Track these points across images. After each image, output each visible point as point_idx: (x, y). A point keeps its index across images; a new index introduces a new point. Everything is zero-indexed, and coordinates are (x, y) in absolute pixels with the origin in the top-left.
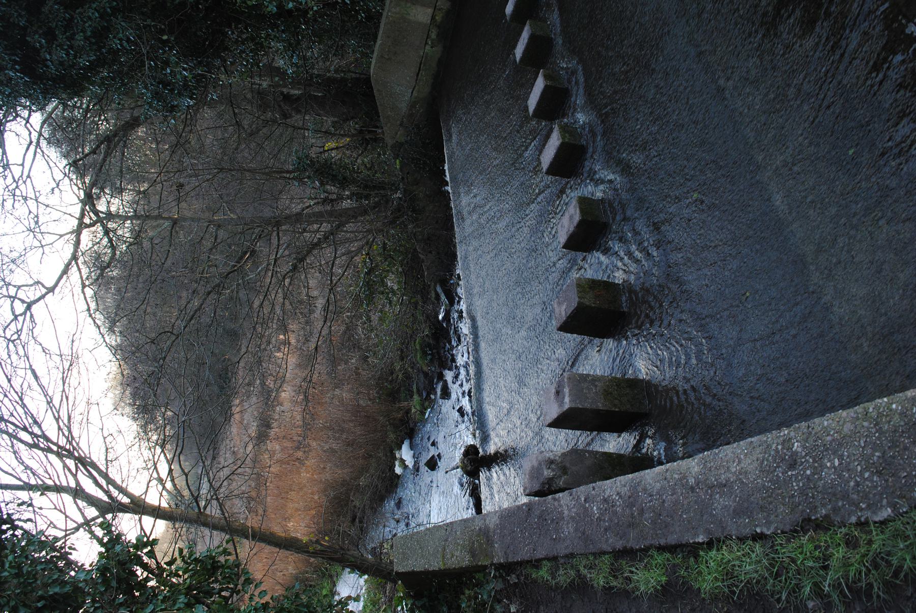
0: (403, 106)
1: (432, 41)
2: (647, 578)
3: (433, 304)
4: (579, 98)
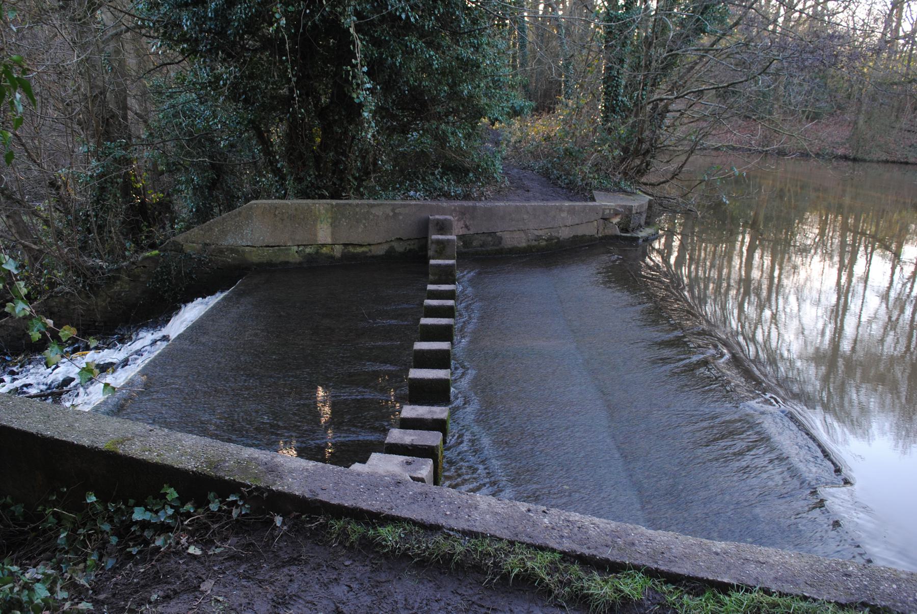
0: (230, 241)
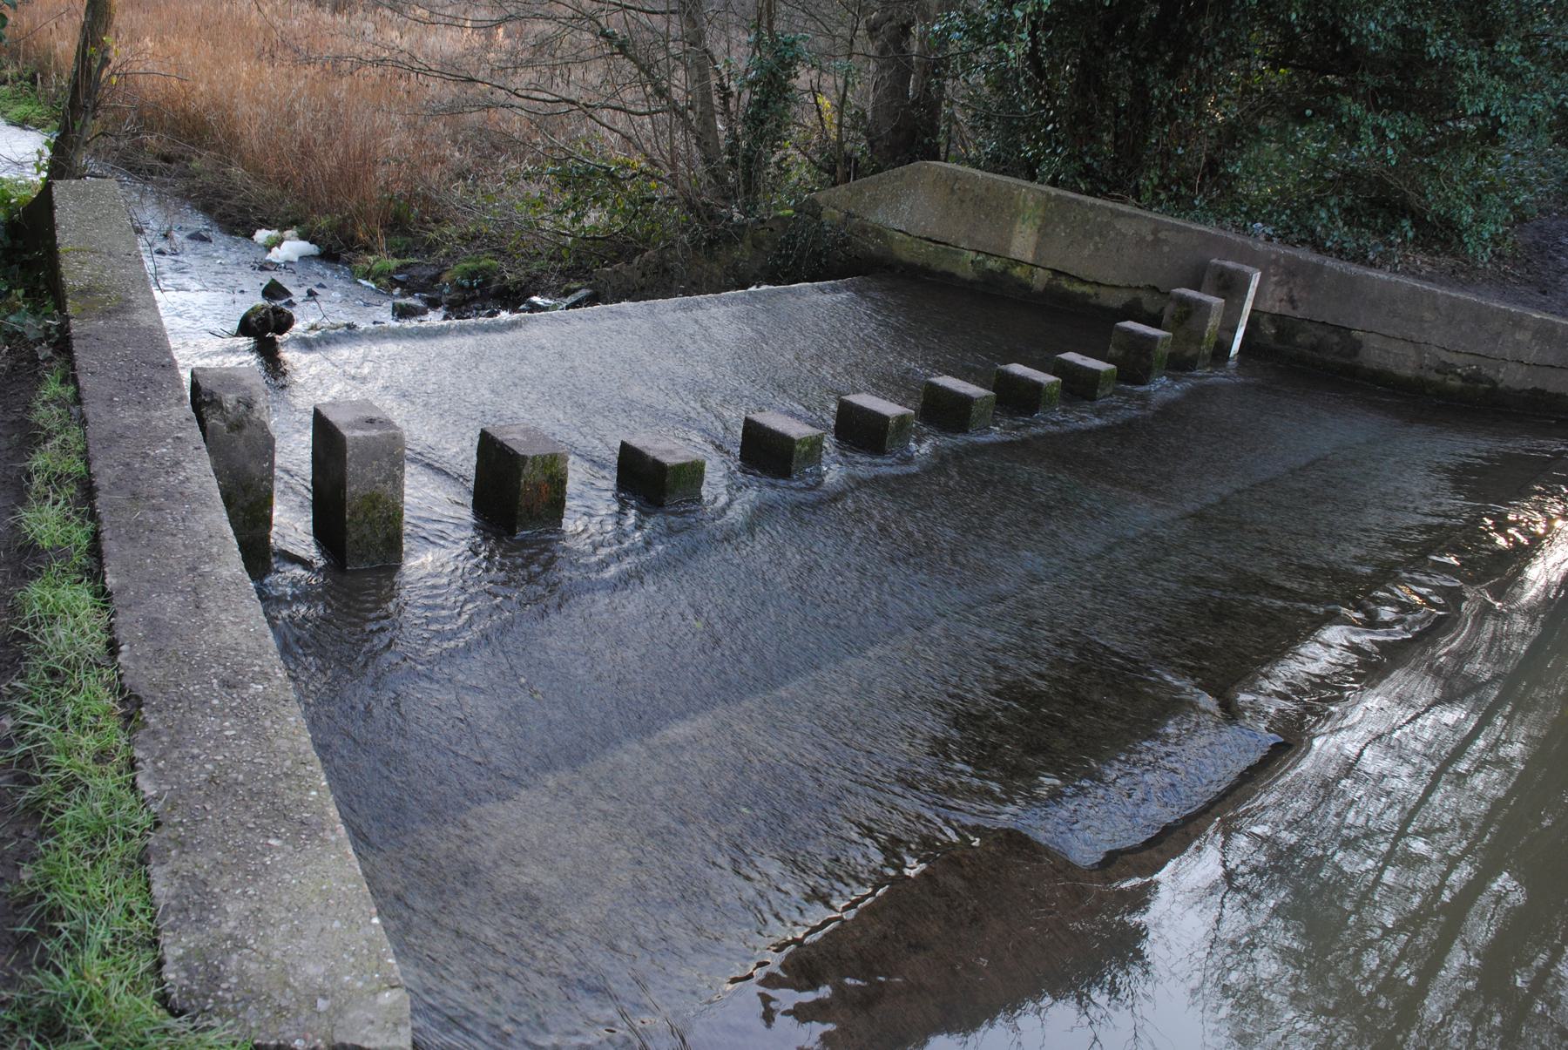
0: (878, 217)
1: (983, 262)
2: (46, 522)
3: (559, 287)
4: (865, 466)
